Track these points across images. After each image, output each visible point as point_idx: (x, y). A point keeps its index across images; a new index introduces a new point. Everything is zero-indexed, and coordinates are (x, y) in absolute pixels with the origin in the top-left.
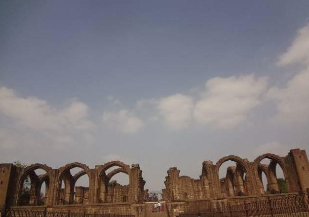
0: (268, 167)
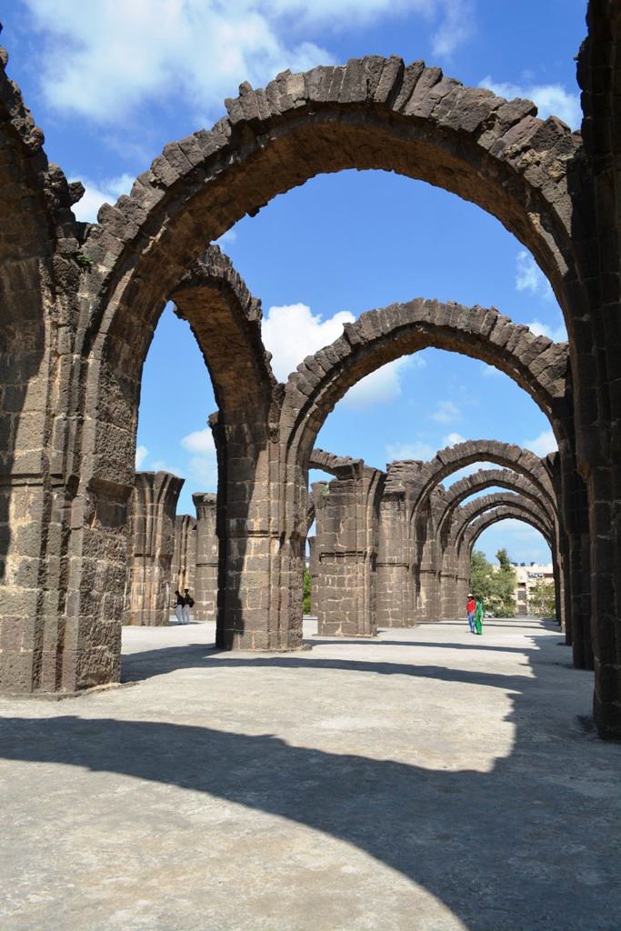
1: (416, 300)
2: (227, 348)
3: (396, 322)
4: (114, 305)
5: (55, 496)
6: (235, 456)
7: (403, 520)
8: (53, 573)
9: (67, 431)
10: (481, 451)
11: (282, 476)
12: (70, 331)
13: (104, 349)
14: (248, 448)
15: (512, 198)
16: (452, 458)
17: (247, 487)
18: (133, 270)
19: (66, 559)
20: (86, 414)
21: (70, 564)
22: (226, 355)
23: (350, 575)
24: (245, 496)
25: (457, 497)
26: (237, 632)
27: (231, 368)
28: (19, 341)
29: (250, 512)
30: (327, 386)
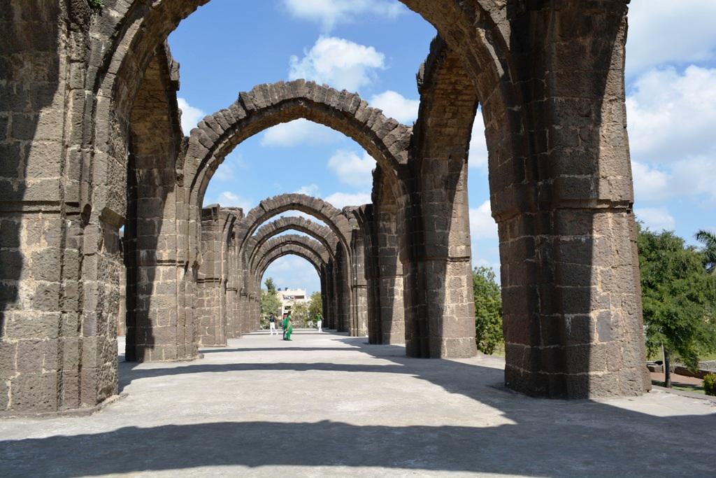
1: (299, 80)
2: (147, 101)
3: (283, 96)
4: (123, 49)
5: (70, 224)
6: (146, 196)
7: (233, 254)
8: (71, 295)
9: (81, 162)
10: (294, 202)
11: (186, 215)
12: (83, 68)
13: (113, 89)
14: (157, 190)
15: (463, 14)
16: (272, 207)
17: (156, 223)
18: (142, 19)
19: (82, 283)
20: (95, 147)
21: (84, 288)
22: (145, 108)
23: (209, 298)
24: (154, 230)
25: (264, 237)
26: (148, 347)
27: (148, 119)
28: (27, 71)
29: (159, 244)
30: (224, 142)
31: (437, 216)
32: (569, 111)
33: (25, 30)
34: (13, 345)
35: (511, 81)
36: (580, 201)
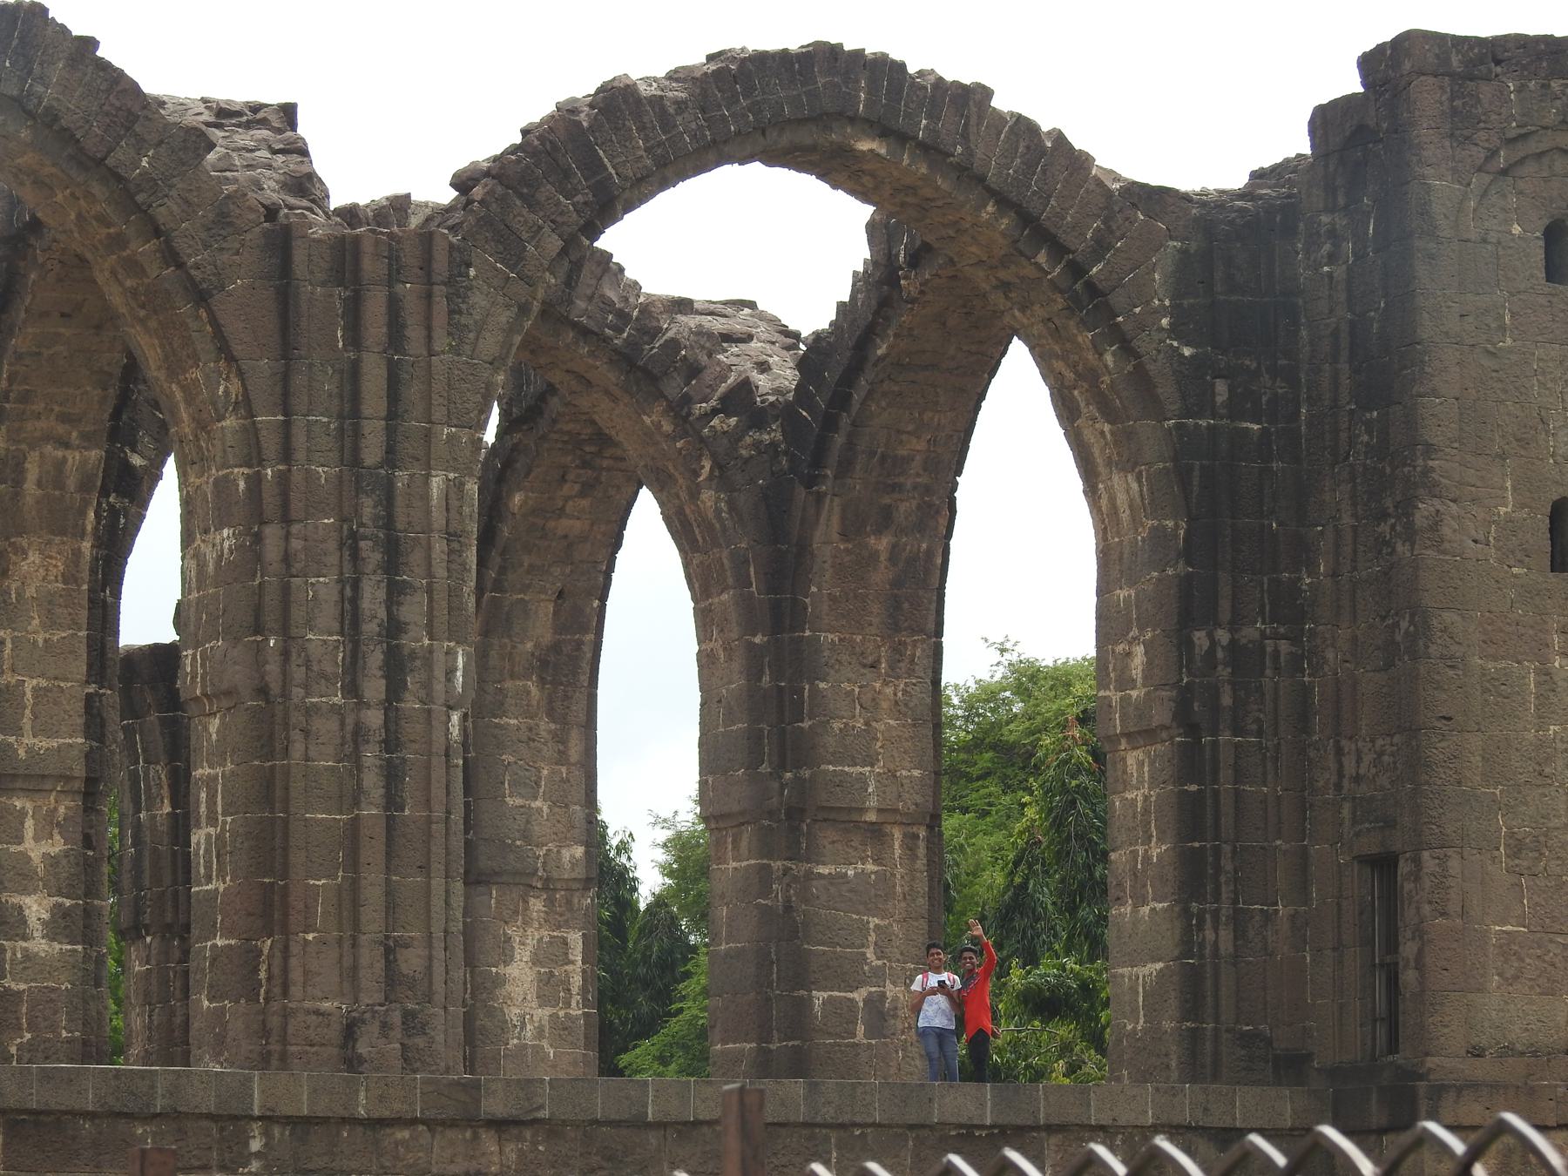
0: (783, 375)
31: (512, 759)
32: (845, 658)
33: (38, 502)
34: (20, 993)
35: (754, 588)
36: (850, 810)
